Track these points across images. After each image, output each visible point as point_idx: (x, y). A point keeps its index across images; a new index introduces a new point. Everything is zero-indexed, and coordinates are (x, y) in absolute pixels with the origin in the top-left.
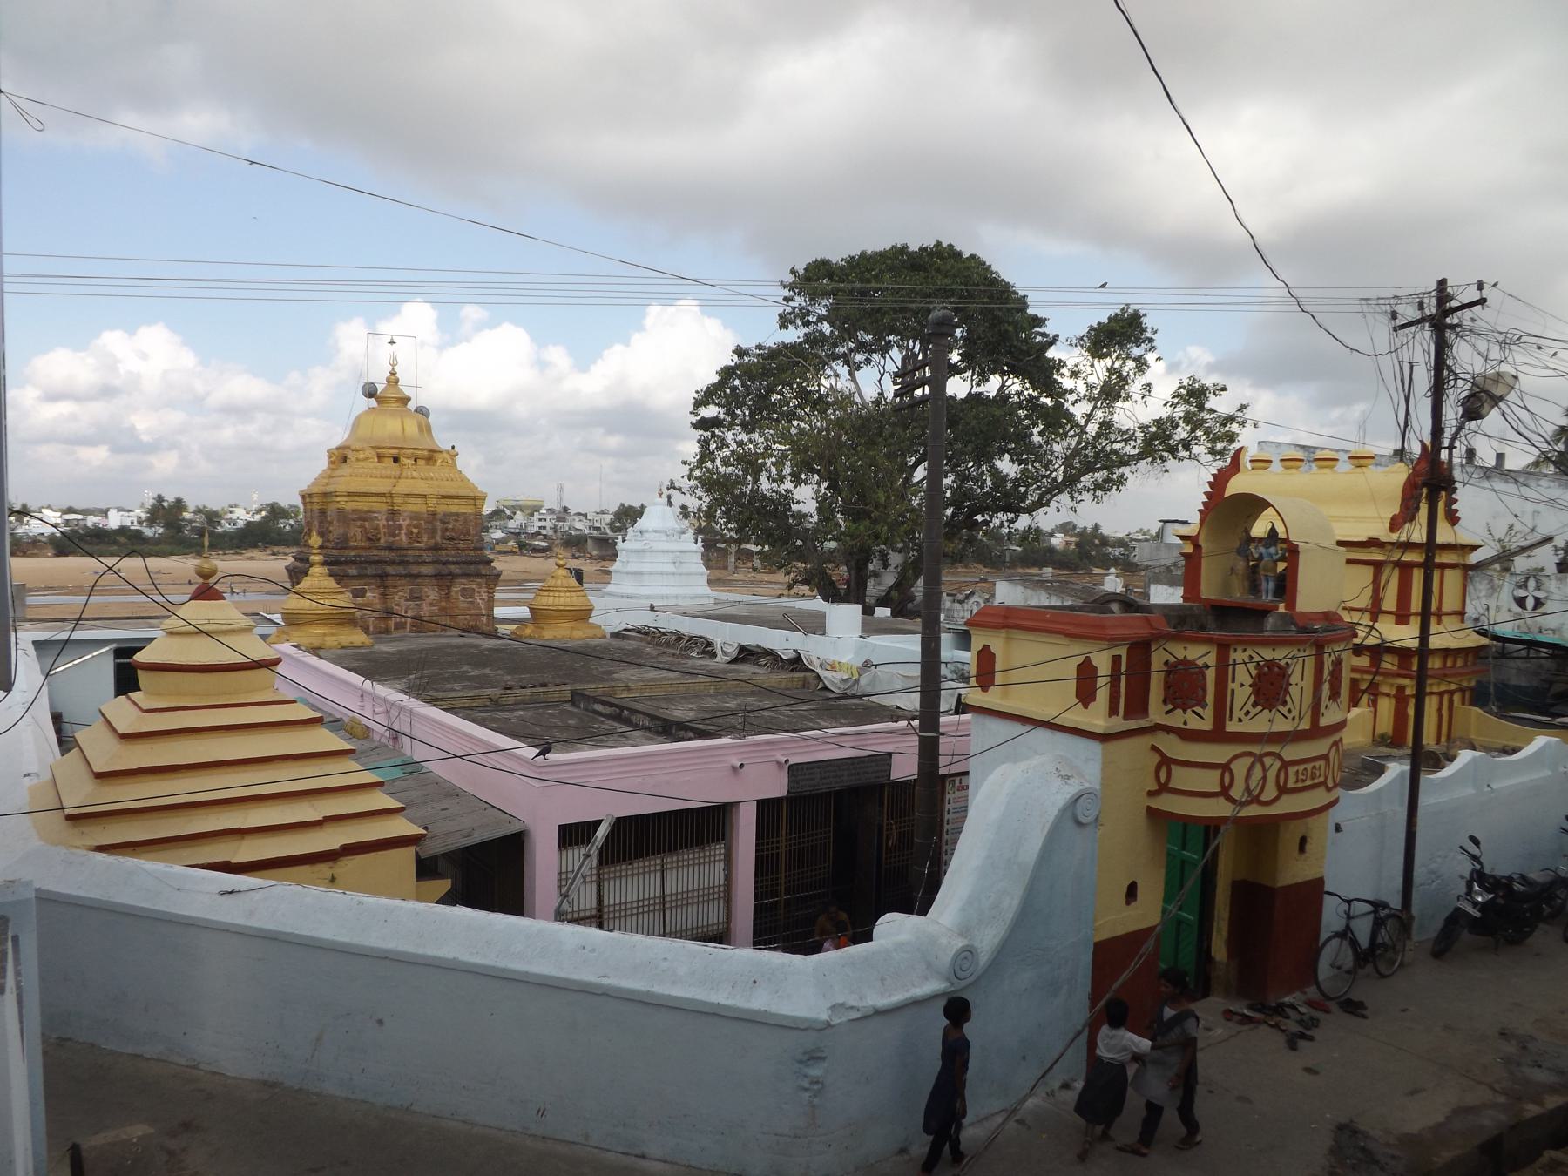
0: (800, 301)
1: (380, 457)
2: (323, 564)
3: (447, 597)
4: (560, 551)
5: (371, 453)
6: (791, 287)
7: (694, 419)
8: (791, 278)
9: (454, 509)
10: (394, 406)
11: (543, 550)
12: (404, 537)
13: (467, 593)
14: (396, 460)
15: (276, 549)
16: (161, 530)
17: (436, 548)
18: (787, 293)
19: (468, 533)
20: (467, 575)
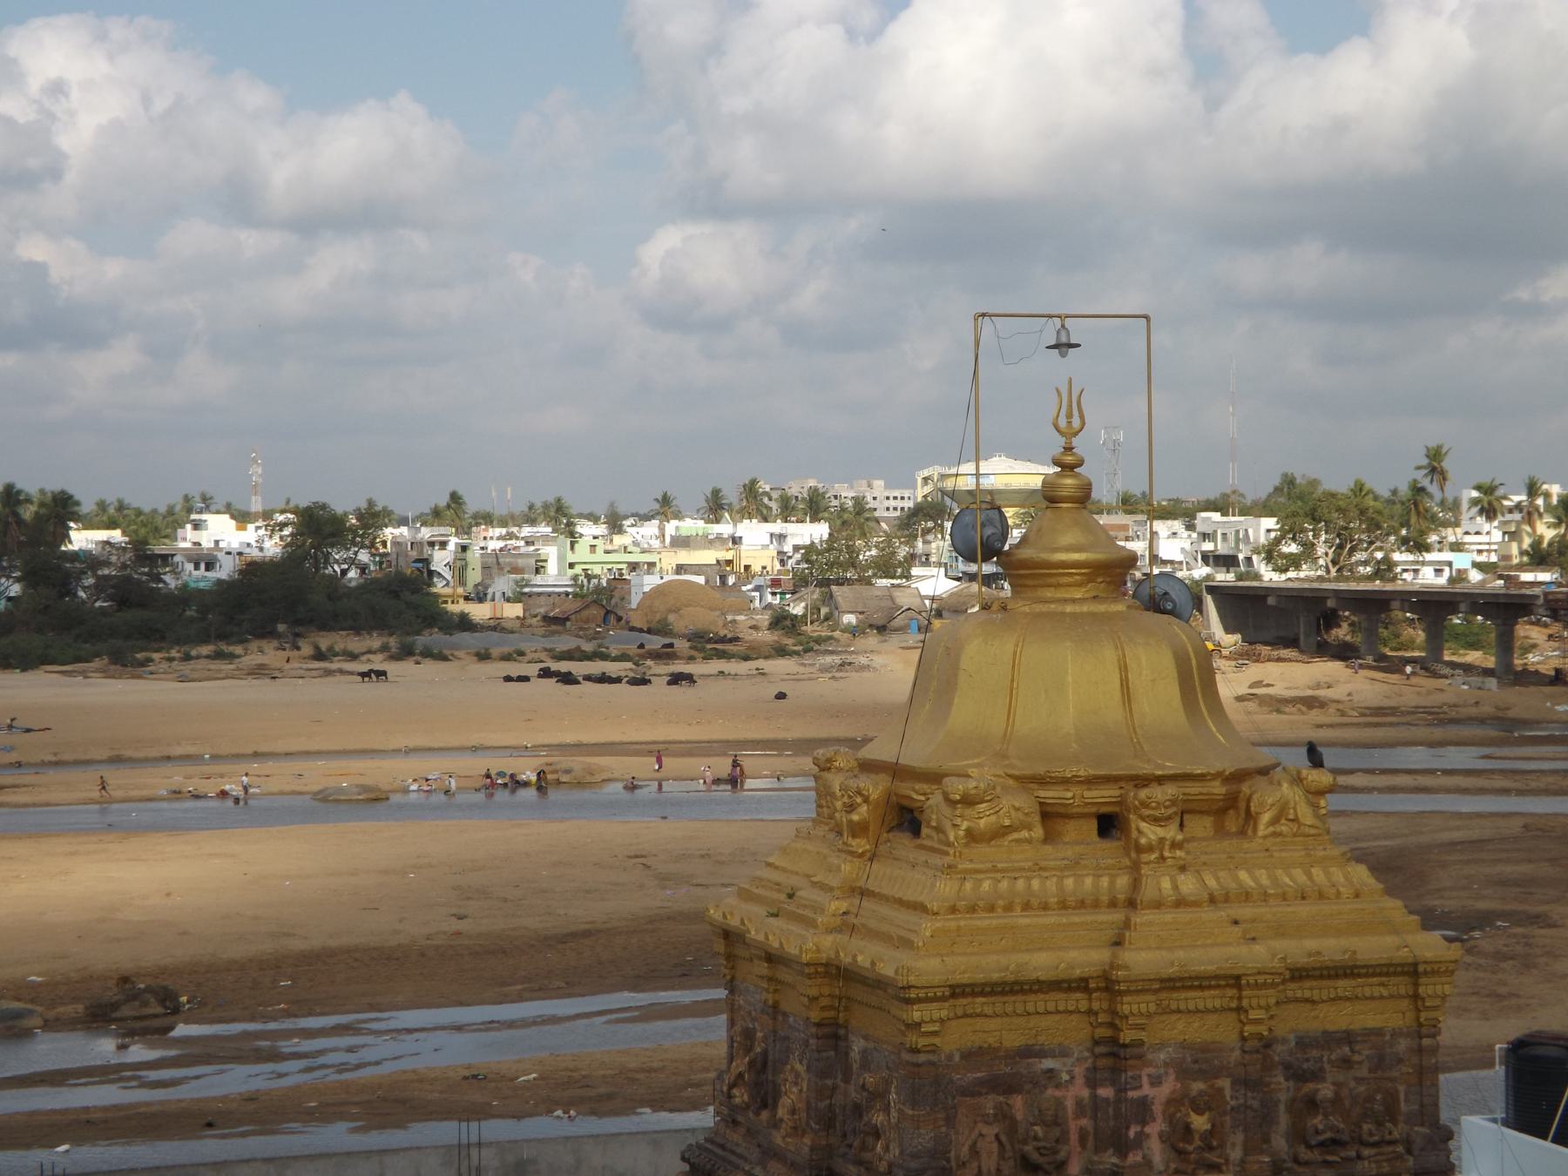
1: (1050, 815)
5: (1015, 805)
9: (1338, 1018)
10: (1077, 599)
14: (1108, 824)
15: (324, 642)
19: (1391, 1112)
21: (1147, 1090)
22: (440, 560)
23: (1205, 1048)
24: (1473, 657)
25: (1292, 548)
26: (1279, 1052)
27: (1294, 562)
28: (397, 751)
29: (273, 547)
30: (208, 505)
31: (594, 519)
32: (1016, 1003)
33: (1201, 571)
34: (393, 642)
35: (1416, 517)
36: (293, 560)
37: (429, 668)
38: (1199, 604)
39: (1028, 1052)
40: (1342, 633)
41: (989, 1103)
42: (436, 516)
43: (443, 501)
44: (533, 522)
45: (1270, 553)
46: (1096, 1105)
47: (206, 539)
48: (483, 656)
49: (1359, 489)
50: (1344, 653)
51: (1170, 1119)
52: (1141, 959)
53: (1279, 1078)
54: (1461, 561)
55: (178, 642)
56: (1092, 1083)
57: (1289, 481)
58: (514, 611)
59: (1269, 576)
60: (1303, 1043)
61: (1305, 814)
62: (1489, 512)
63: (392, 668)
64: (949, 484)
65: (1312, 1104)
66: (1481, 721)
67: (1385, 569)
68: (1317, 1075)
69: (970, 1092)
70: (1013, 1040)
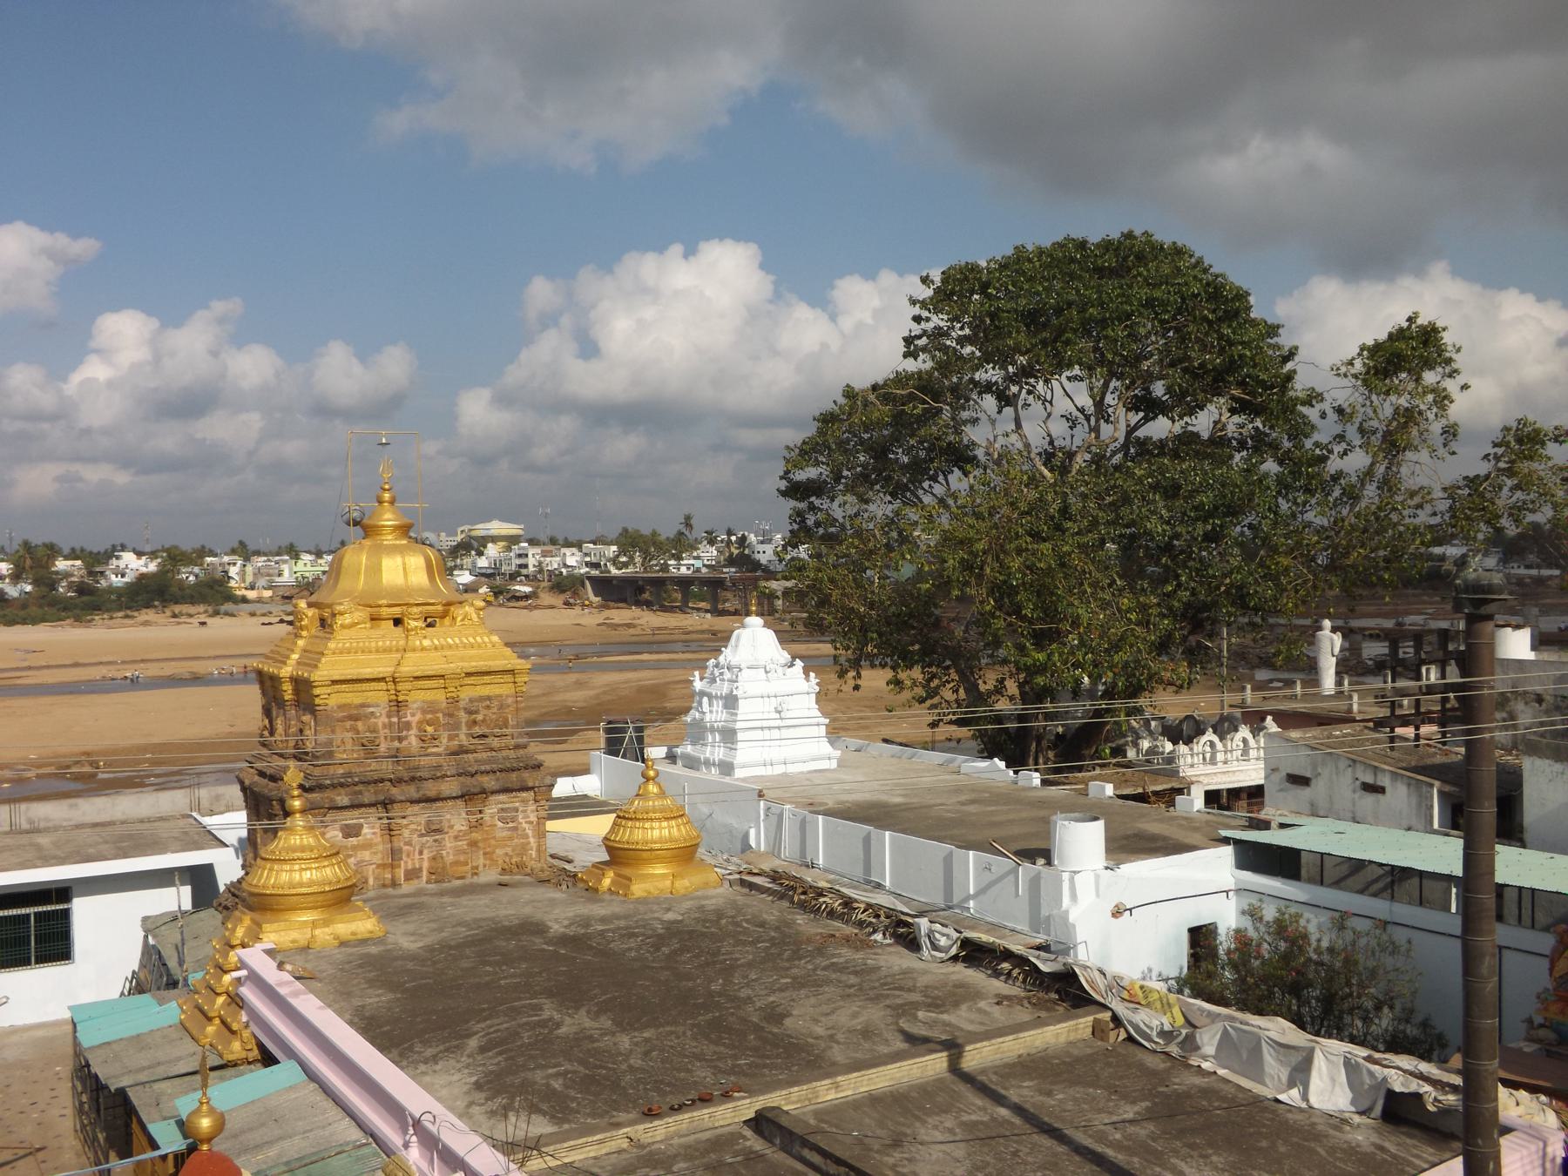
0: (938, 320)
2: (303, 811)
3: (477, 825)
4: (547, 598)
6: (923, 304)
7: (783, 485)
8: (927, 293)
11: (526, 597)
12: (414, 741)
13: (507, 816)
14: (397, 622)
15: (177, 609)
16: (29, 588)
17: (462, 751)
18: (917, 310)
20: (506, 790)
21: (409, 718)
22: (233, 571)
23: (432, 702)
24: (702, 605)
25: (624, 559)
26: (462, 704)
27: (625, 565)
28: (209, 658)
29: (153, 567)
30: (123, 548)
31: (309, 552)
32: (358, 686)
33: (584, 570)
34: (210, 609)
35: (681, 544)
36: (162, 573)
37: (227, 620)
38: (583, 585)
39: (363, 706)
40: (646, 596)
41: (348, 724)
42: (233, 552)
43: (236, 545)
44: (278, 554)
45: (614, 561)
46: (391, 725)
47: (122, 564)
48: (253, 614)
49: (654, 534)
50: (648, 604)
51: (420, 730)
52: (407, 669)
53: (462, 713)
54: (698, 564)
55: (108, 611)
56: (389, 716)
57: (625, 530)
58: (268, 594)
59: (614, 571)
60: (471, 701)
61: (474, 616)
62: (712, 542)
63: (209, 621)
64: (474, 533)
65: (475, 722)
66: (702, 632)
67: (665, 568)
68: (477, 712)
69: (342, 720)
70: (357, 701)
